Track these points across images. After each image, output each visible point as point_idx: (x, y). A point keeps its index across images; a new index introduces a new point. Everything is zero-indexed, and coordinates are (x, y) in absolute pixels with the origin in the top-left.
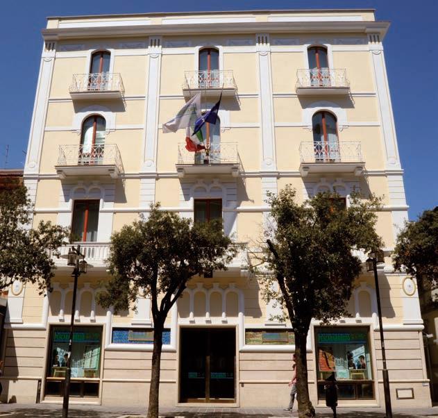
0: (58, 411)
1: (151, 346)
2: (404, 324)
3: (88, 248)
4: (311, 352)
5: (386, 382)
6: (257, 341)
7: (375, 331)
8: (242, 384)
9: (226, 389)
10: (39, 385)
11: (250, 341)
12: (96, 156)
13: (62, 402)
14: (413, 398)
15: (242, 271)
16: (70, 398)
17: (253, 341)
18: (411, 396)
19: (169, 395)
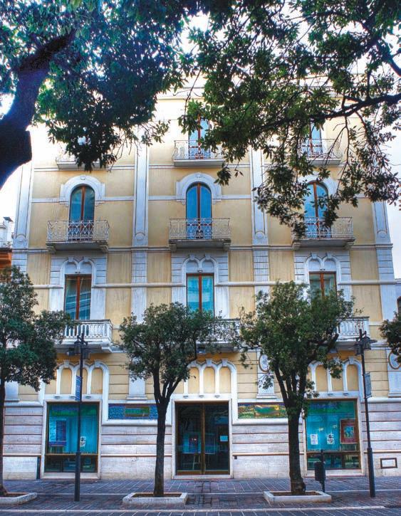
0: (151, 481)
1: (155, 422)
2: (390, 397)
3: (86, 326)
4: (302, 424)
5: (370, 453)
6: (250, 415)
7: (361, 403)
8: (236, 457)
9: (220, 461)
10: (39, 462)
11: (243, 415)
12: (87, 233)
13: (74, 477)
14: (381, 460)
15: (281, 375)
16: (326, 471)
17: (246, 415)
18: (383, 461)
19: (170, 466)
